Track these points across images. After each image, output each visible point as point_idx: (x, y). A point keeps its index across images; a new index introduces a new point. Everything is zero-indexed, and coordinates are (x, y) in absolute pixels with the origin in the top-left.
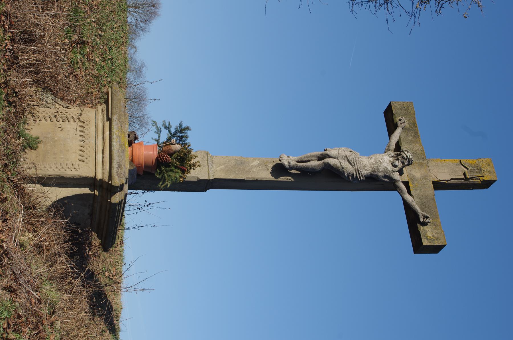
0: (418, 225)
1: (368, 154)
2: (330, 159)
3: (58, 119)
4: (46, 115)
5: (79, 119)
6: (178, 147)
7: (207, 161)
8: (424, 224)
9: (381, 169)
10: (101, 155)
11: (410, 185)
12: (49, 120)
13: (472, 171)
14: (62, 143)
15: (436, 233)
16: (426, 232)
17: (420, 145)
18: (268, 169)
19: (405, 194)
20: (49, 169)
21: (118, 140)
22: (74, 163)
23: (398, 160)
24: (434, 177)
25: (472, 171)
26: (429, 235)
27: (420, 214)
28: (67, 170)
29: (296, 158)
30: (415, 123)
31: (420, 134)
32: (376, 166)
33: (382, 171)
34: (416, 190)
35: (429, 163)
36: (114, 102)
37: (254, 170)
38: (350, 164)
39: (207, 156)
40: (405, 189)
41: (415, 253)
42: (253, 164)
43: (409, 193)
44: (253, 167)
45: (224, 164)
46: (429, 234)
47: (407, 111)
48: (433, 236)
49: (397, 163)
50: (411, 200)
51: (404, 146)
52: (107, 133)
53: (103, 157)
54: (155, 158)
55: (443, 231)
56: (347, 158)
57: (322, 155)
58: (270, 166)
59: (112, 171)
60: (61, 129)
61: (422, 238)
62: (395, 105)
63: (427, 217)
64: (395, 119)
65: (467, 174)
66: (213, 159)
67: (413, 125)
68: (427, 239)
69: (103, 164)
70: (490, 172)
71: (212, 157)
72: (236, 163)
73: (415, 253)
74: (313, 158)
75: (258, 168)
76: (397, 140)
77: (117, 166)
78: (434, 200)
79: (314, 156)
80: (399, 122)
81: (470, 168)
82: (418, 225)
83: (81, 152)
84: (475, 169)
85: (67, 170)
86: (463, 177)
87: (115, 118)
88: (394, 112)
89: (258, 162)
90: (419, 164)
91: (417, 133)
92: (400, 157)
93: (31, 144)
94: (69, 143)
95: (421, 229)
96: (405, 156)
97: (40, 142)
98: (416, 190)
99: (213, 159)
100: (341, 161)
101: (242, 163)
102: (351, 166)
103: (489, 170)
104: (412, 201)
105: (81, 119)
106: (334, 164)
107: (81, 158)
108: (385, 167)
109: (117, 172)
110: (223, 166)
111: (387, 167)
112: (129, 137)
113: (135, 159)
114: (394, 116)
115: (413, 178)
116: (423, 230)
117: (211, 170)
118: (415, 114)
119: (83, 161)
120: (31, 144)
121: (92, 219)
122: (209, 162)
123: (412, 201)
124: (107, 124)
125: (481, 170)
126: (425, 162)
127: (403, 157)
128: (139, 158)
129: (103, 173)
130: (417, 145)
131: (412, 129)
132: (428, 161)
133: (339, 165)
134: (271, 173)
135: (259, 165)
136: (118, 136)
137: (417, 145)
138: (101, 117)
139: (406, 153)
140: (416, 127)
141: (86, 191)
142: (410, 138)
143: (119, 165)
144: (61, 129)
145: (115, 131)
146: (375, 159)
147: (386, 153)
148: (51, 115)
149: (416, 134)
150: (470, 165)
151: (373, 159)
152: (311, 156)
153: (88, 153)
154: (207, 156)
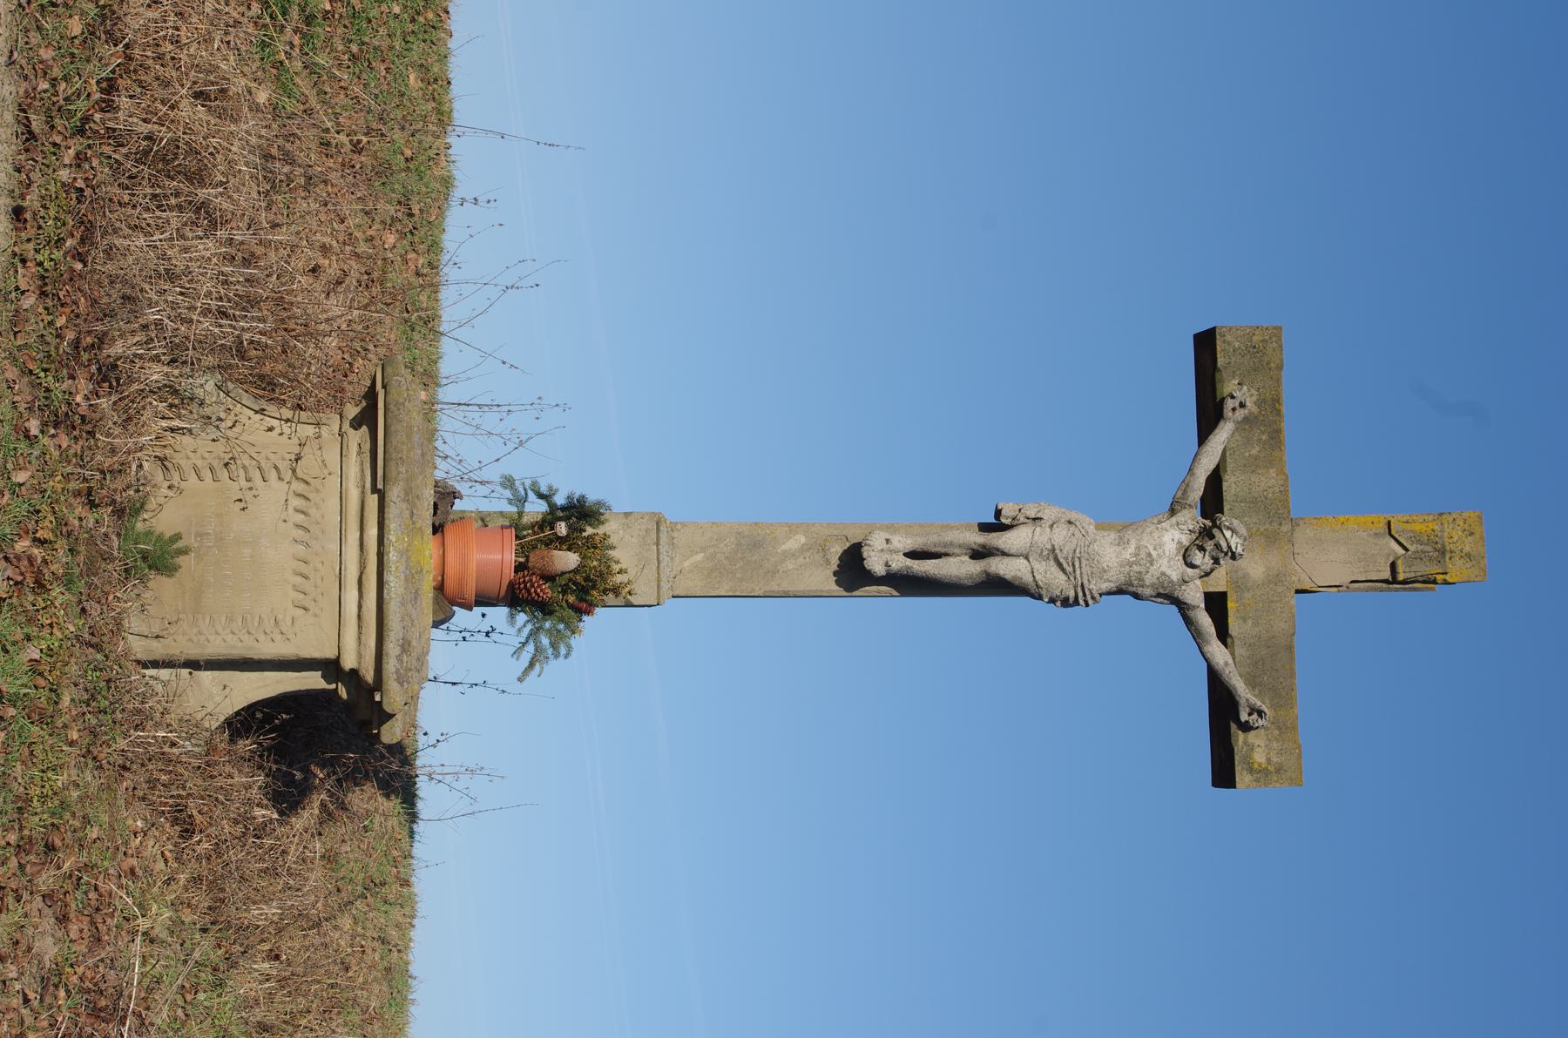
0: (1233, 726)
1: (1123, 529)
2: (1006, 560)
3: (234, 476)
4: (199, 463)
5: (294, 471)
6: (567, 560)
7: (658, 544)
8: (1246, 728)
9: (1148, 580)
10: (356, 593)
11: (1230, 604)
12: (207, 475)
13: (1419, 557)
14: (247, 551)
15: (1280, 752)
16: (1252, 748)
17: (1281, 472)
18: (828, 562)
19: (1208, 642)
20: (212, 638)
21: (402, 568)
22: (280, 617)
23: (1202, 549)
24: (1303, 576)
25: (1419, 557)
26: (1259, 757)
27: (1242, 702)
28: (262, 637)
29: (910, 543)
30: (1277, 400)
31: (1287, 436)
32: (1136, 568)
33: (1152, 585)
34: (1244, 620)
35: (1298, 533)
36: (394, 441)
37: (790, 565)
38: (1063, 570)
39: (658, 530)
40: (1213, 630)
41: (1214, 785)
42: (784, 547)
43: (1223, 635)
44: (787, 555)
45: (703, 549)
46: (1254, 747)
47: (1264, 356)
48: (1269, 761)
49: (1198, 558)
50: (1221, 662)
51: (1233, 479)
52: (372, 532)
53: (360, 607)
54: (505, 583)
55: (1299, 747)
56: (1053, 555)
57: (984, 546)
58: (837, 550)
59: (385, 666)
60: (242, 505)
61: (1238, 768)
62: (1228, 338)
63: (1260, 713)
64: (1218, 386)
65: (1400, 568)
66: (675, 534)
67: (1272, 404)
68: (1251, 771)
69: (360, 627)
70: (1469, 555)
71: (673, 527)
72: (739, 544)
73: (1214, 785)
74: (957, 551)
75: (801, 560)
76: (1212, 467)
77: (397, 651)
78: (1290, 649)
79: (960, 546)
80: (1230, 404)
81: (1412, 548)
82: (1233, 726)
83: (299, 579)
84: (1429, 548)
85: (262, 637)
86: (1387, 575)
87: (395, 494)
88: (1221, 361)
89: (803, 540)
90: (1267, 537)
91: (1279, 431)
92: (1209, 545)
93: (160, 559)
94: (262, 553)
95: (1239, 738)
96: (1224, 544)
97: (184, 552)
98: (1244, 620)
99: (675, 534)
100: (1036, 565)
101: (756, 545)
102: (1064, 577)
103: (1467, 549)
104: (1226, 664)
105: (299, 473)
106: (1015, 577)
107: (302, 568)
108: (1163, 574)
109: (397, 672)
110: (700, 557)
111: (1168, 572)
112: (435, 514)
113: (450, 585)
114: (1218, 376)
115: (1240, 583)
116: (1245, 742)
117: (666, 572)
118: (1280, 368)
119: (306, 578)
120: (160, 559)
121: (330, 738)
122: (662, 550)
123: (1226, 664)
124: (373, 501)
125: (1443, 552)
126: (1285, 528)
127: (1218, 546)
128: (461, 582)
129: (360, 656)
130: (1273, 472)
131: (1267, 422)
132: (1294, 523)
133: (1028, 578)
134: (835, 574)
135: (804, 549)
136: (401, 553)
137: (1273, 472)
138: (355, 468)
139: (1228, 534)
140: (1279, 413)
141: (313, 681)
142: (1254, 452)
143: (402, 646)
144: (242, 505)
145: (393, 538)
146: (1138, 548)
147: (1174, 520)
148: (215, 463)
149: (1276, 436)
150: (1416, 538)
151: (1132, 549)
152: (952, 544)
153: (319, 582)
154: (658, 530)
